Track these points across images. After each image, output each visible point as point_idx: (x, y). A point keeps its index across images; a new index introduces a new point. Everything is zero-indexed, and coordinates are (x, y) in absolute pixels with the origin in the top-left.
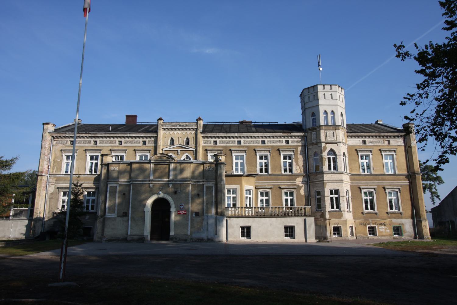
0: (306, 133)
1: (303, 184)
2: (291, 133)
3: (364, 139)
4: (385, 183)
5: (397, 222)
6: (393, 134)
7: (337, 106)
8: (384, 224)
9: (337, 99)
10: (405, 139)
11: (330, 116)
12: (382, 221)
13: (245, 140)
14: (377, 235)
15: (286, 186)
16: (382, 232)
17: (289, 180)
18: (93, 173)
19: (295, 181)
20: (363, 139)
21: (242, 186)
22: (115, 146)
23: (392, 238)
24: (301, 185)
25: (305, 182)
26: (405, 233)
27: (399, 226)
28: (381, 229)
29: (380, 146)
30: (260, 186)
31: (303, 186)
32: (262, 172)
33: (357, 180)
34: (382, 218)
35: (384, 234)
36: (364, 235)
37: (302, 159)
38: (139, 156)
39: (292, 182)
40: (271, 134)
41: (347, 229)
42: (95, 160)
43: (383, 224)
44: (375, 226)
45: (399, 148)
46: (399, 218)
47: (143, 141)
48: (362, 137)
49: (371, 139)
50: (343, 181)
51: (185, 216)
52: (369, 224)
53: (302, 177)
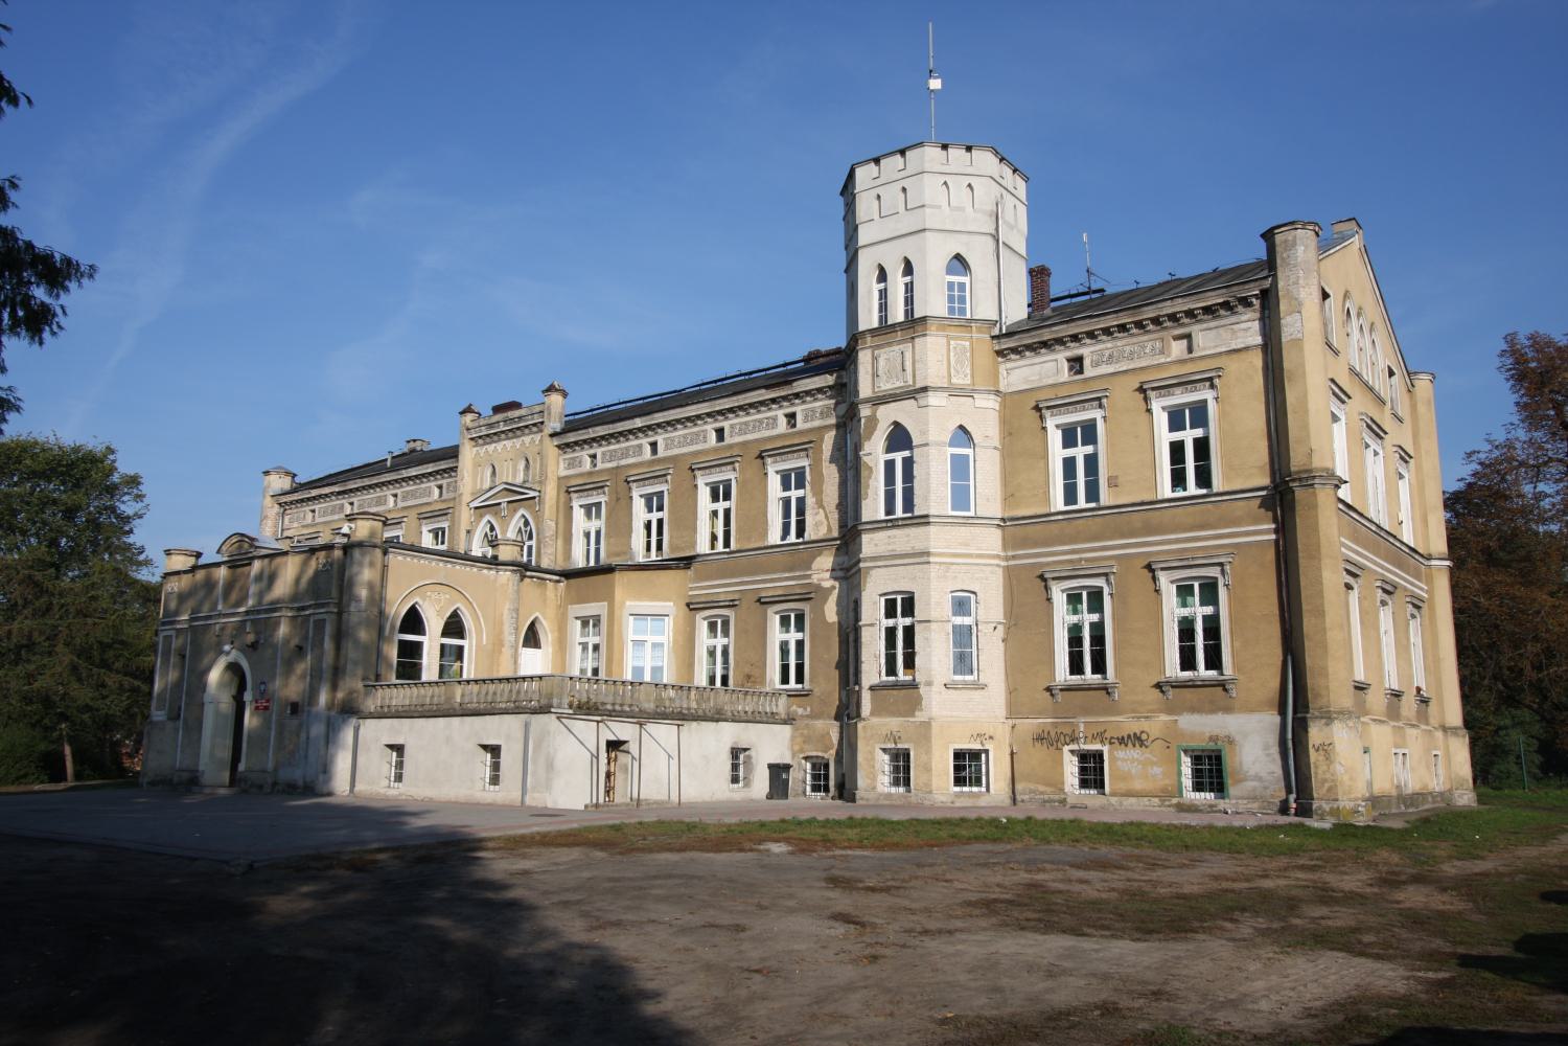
0: (844, 373)
1: (836, 579)
2: (795, 384)
3: (1075, 350)
4: (1158, 545)
5: (1201, 726)
6: (1133, 315)
7: (922, 234)
8: (1139, 739)
9: (923, 206)
10: (1267, 312)
11: (897, 284)
12: (1131, 726)
13: (667, 436)
14: (1107, 789)
15: (780, 593)
16: (1126, 777)
17: (791, 570)
18: (1082, 503)
19: (810, 568)
20: (1069, 354)
21: (613, 605)
22: (640, 464)
23: (1169, 806)
24: (827, 584)
25: (841, 569)
26: (1240, 781)
27: (1211, 746)
28: (1124, 760)
29: (1142, 368)
30: (703, 600)
31: (833, 587)
32: (1075, 503)
33: (1036, 544)
34: (1134, 711)
35: (1138, 785)
36: (1049, 790)
37: (837, 480)
38: (1060, 432)
39: (797, 574)
40: (579, 435)
41: (930, 758)
42: (1191, 428)
43: (1137, 740)
44: (1096, 747)
45: (1233, 366)
46: (1214, 709)
47: (786, 415)
48: (1060, 341)
49: (1106, 345)
50: (928, 554)
51: (268, 712)
52: (1074, 740)
53: (834, 550)
